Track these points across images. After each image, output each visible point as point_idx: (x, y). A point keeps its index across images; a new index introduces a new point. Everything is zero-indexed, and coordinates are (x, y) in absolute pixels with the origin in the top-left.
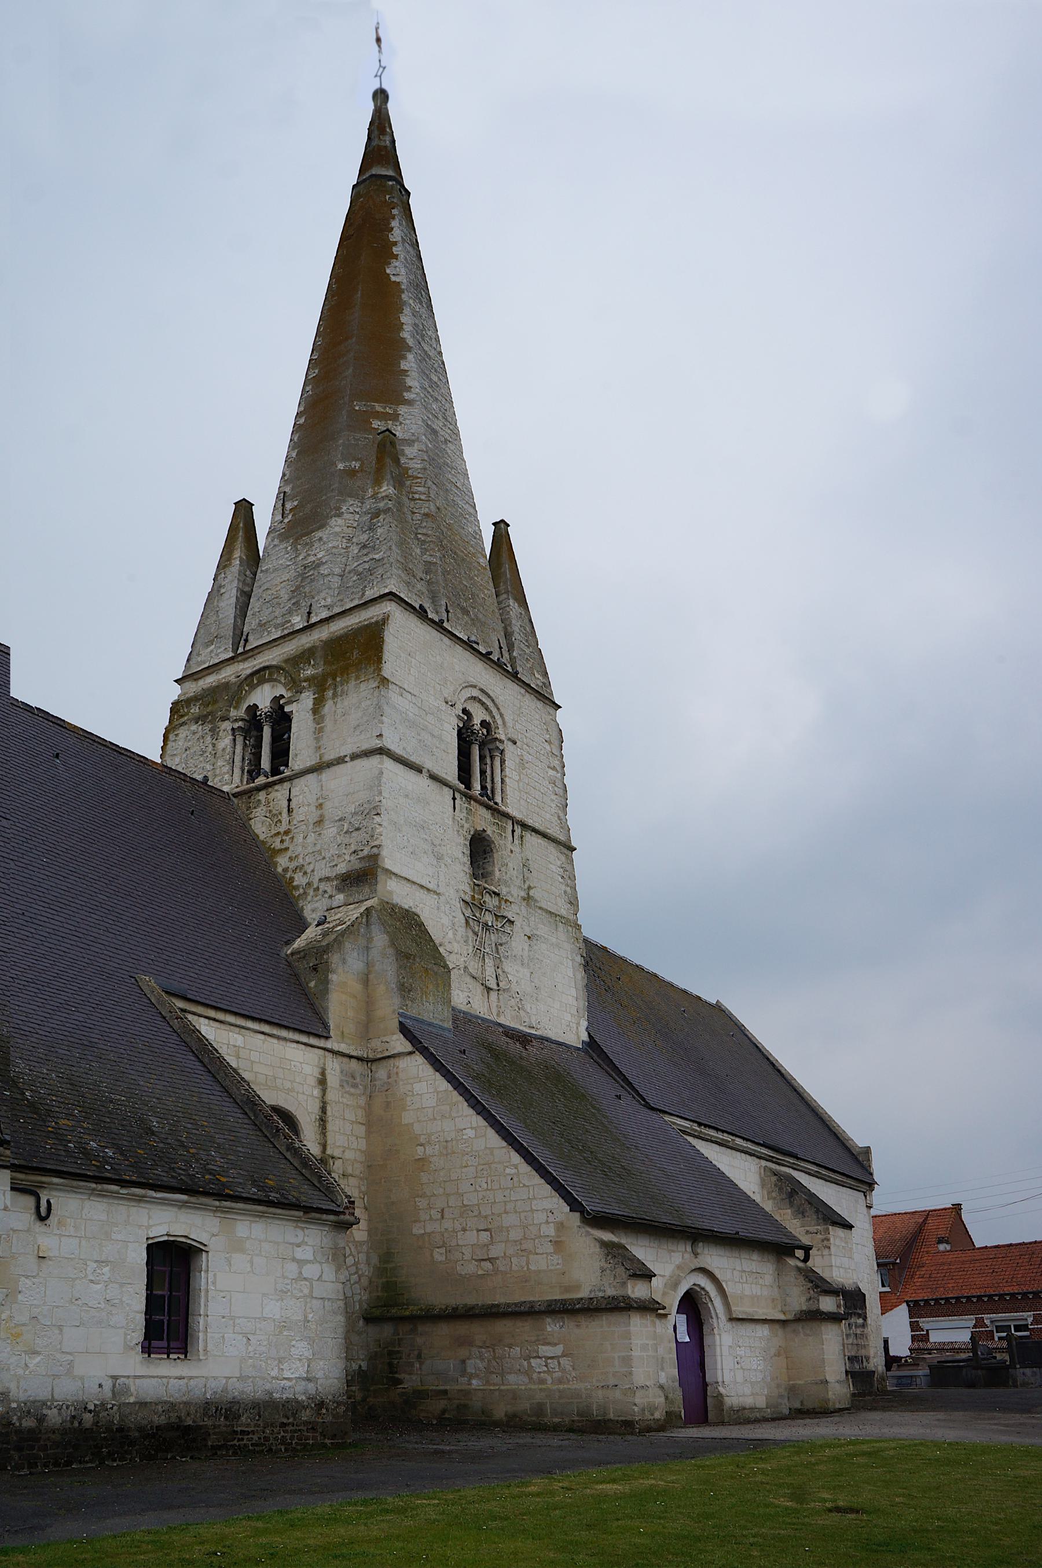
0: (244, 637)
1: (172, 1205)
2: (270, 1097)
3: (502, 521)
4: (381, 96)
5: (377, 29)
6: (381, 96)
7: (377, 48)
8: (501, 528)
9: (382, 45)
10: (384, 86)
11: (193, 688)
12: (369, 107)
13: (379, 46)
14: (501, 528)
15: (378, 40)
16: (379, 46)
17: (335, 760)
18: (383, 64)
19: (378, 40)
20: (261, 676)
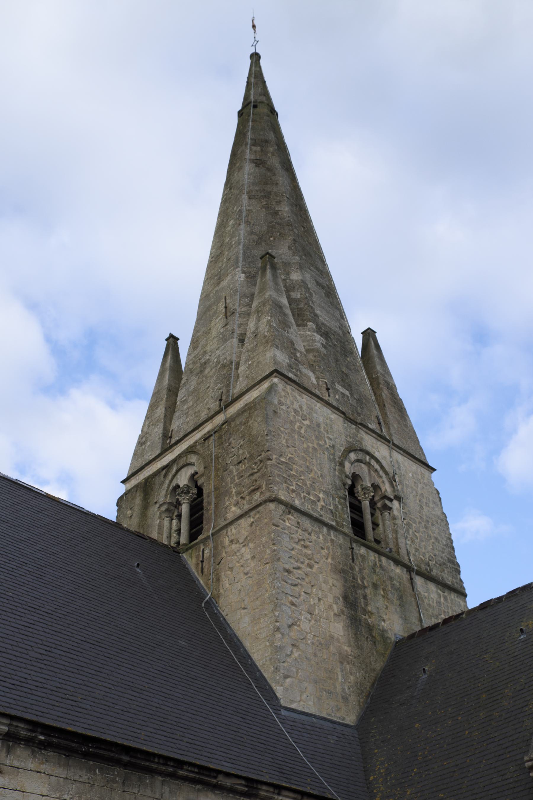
0: (383, 424)
1: (86, 755)
2: (117, 508)
3: (369, 329)
4: (255, 57)
5: (253, 21)
6: (255, 57)
7: (253, 31)
8: (369, 335)
9: (256, 29)
10: (257, 51)
11: (133, 482)
12: (248, 62)
13: (255, 30)
14: (369, 335)
15: (254, 26)
16: (255, 30)
17: (201, 518)
18: (257, 39)
19: (254, 26)
20: (179, 464)
